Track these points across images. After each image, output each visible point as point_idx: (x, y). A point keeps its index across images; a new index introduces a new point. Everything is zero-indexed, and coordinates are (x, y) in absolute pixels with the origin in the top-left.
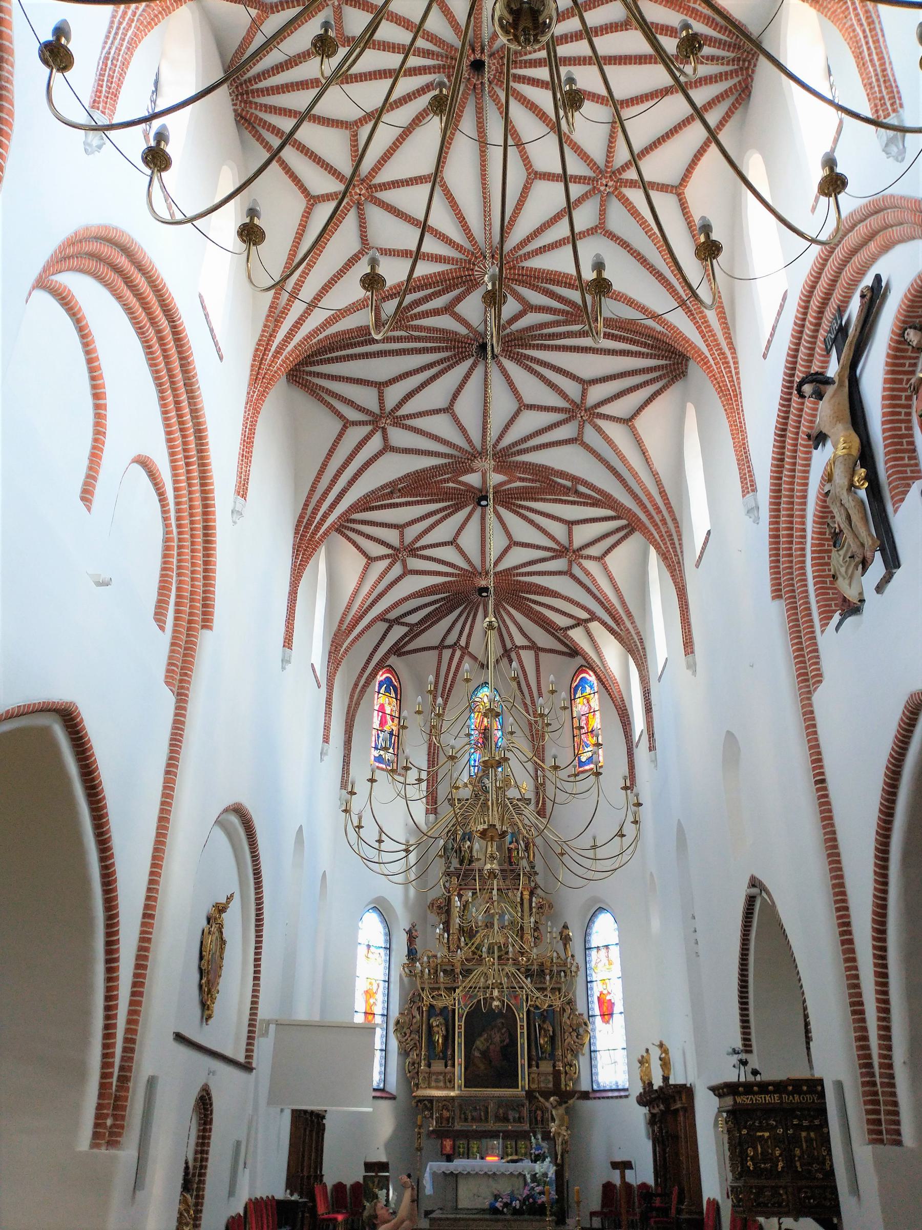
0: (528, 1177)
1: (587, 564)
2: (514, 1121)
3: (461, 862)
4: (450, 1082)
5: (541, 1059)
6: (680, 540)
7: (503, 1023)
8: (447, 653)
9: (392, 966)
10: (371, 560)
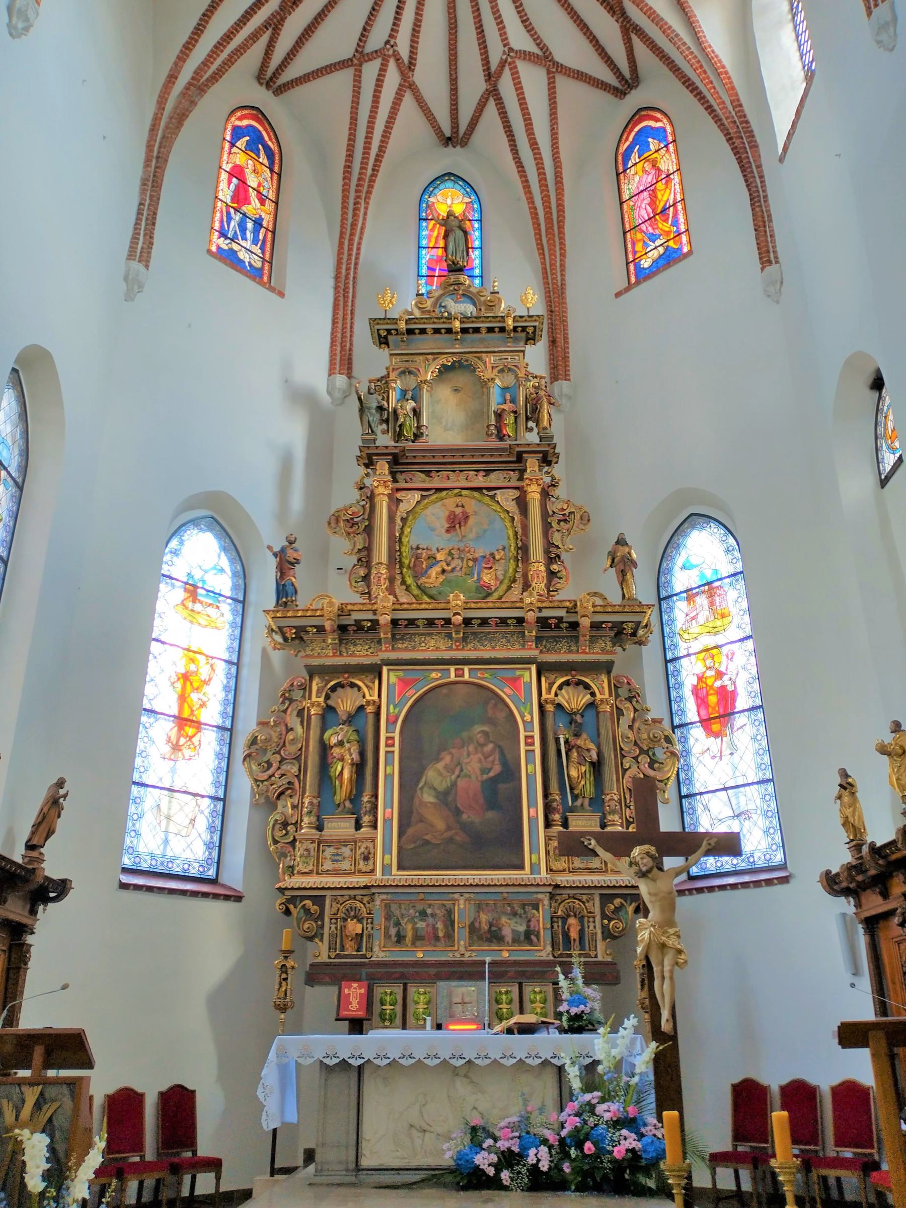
0: (573, 1074)
2: (515, 941)
3: (399, 436)
4: (366, 859)
5: (572, 810)
7: (485, 734)
8: (371, 70)
9: (248, 634)
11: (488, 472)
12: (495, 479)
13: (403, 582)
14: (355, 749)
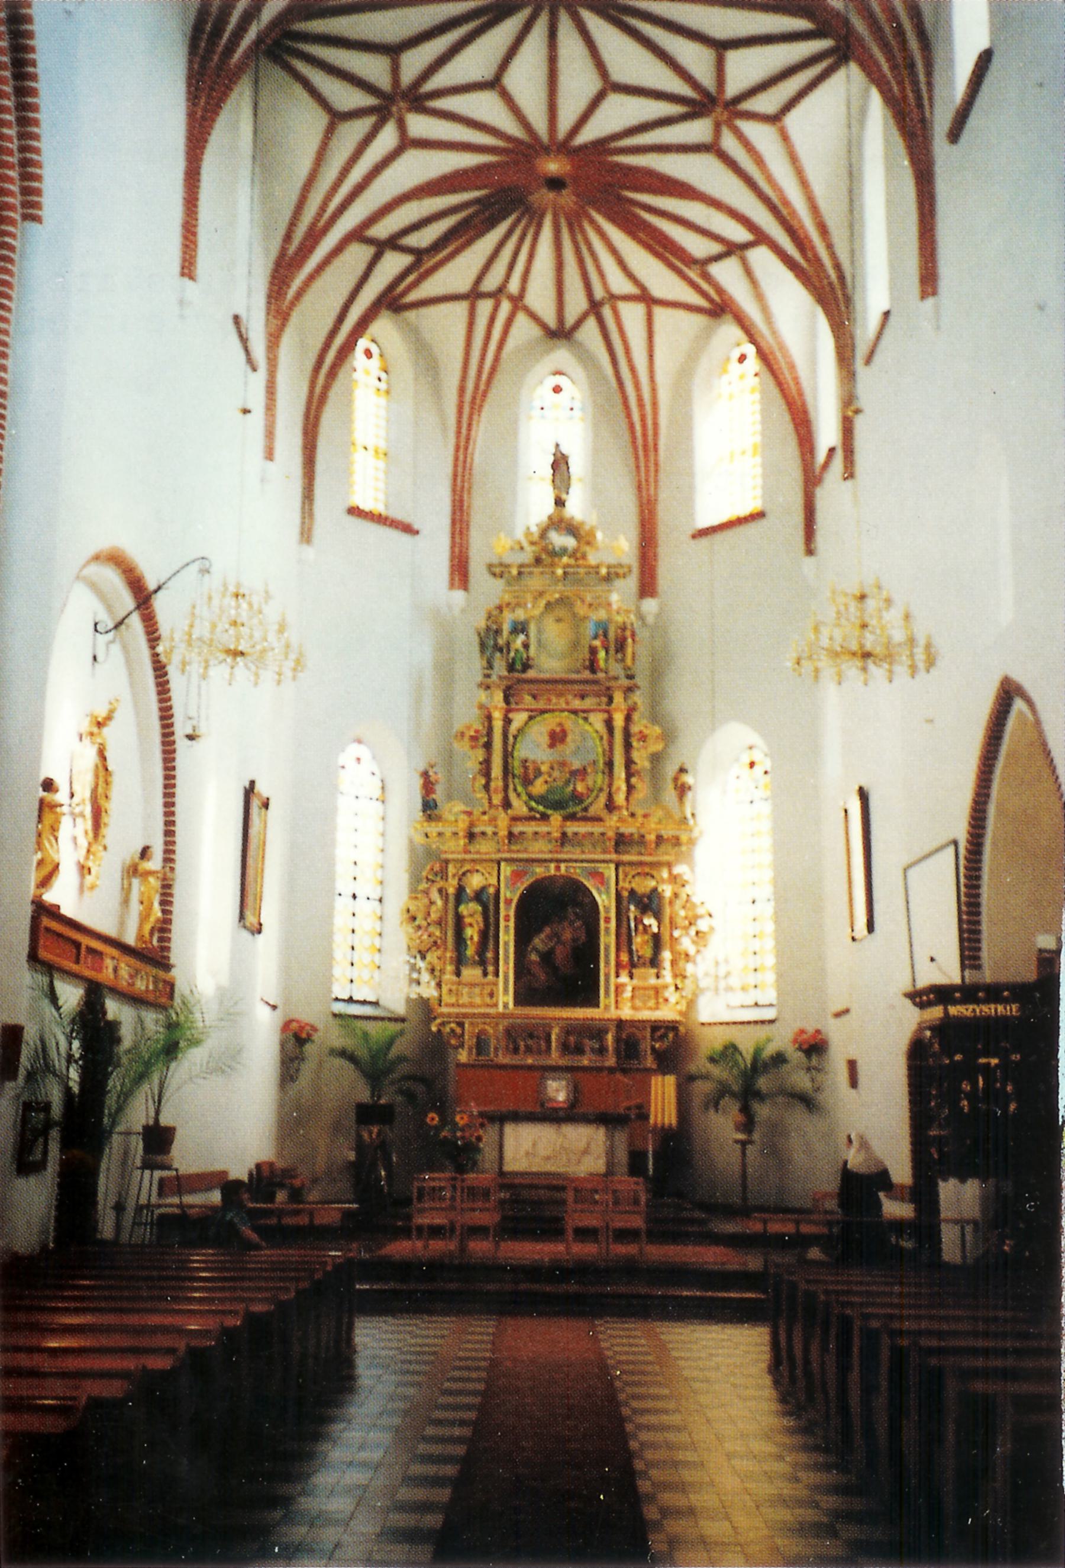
1: (747, 127)
3: (511, 668)
6: (929, 74)
8: (485, 307)
10: (337, 117)
11: (583, 697)
12: (589, 703)
13: (515, 790)
14: (480, 919)
